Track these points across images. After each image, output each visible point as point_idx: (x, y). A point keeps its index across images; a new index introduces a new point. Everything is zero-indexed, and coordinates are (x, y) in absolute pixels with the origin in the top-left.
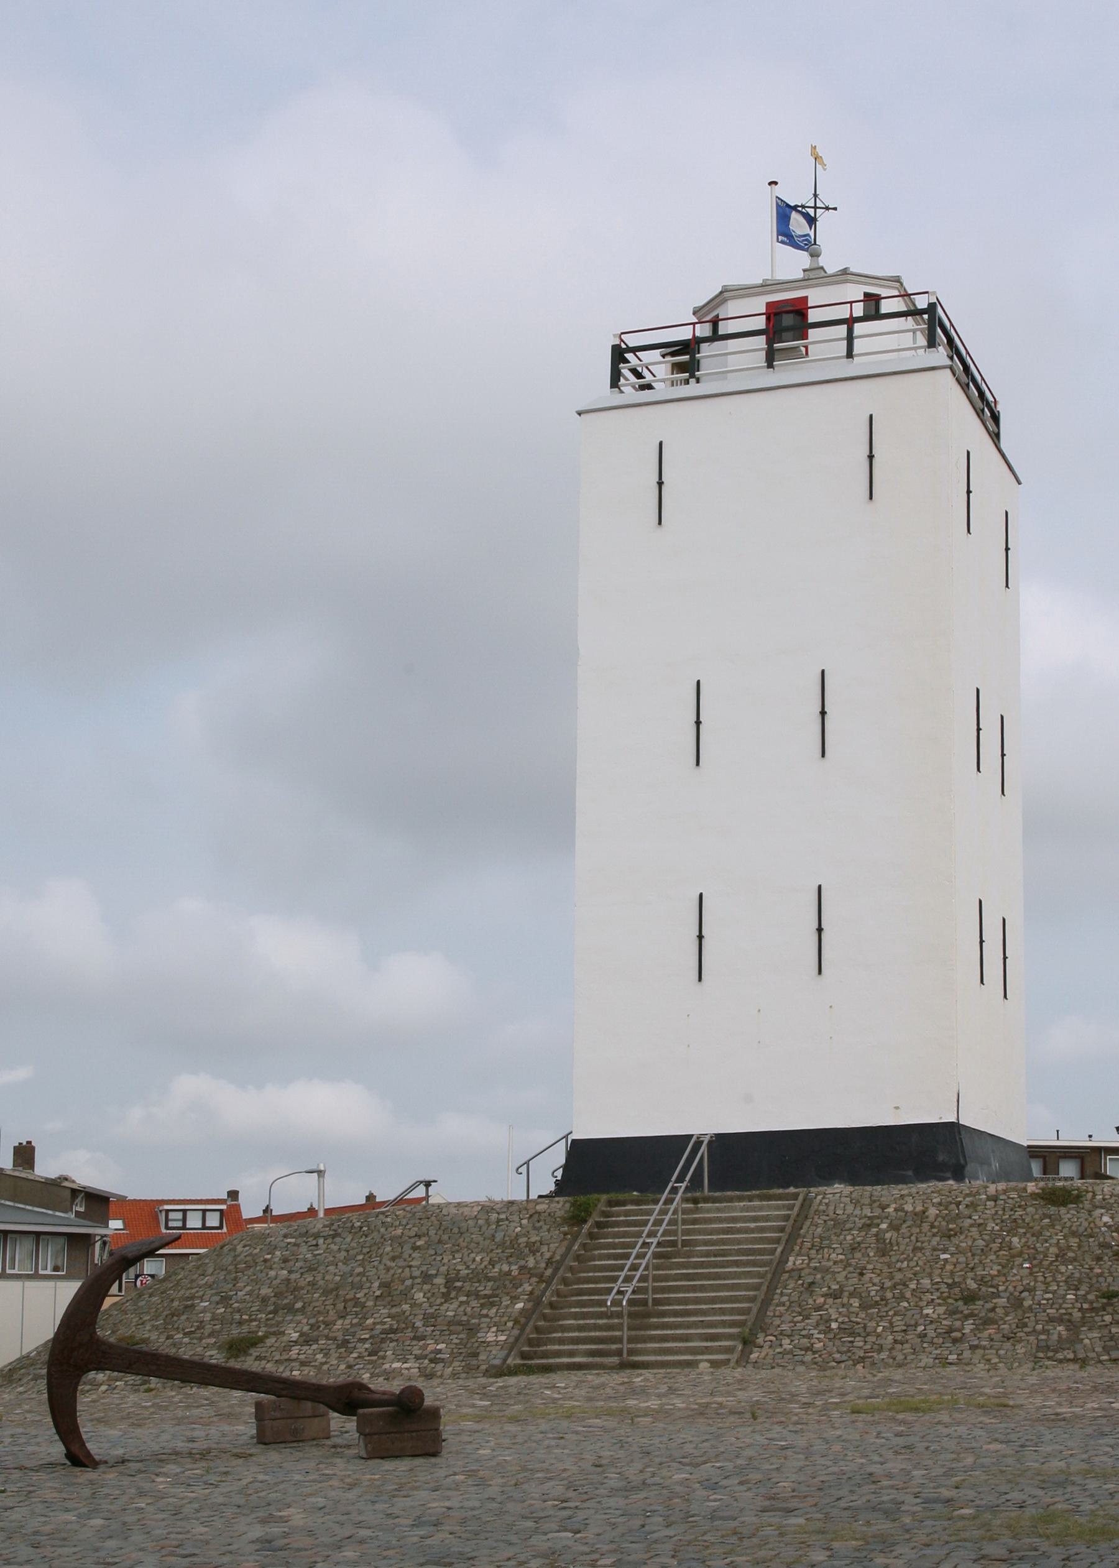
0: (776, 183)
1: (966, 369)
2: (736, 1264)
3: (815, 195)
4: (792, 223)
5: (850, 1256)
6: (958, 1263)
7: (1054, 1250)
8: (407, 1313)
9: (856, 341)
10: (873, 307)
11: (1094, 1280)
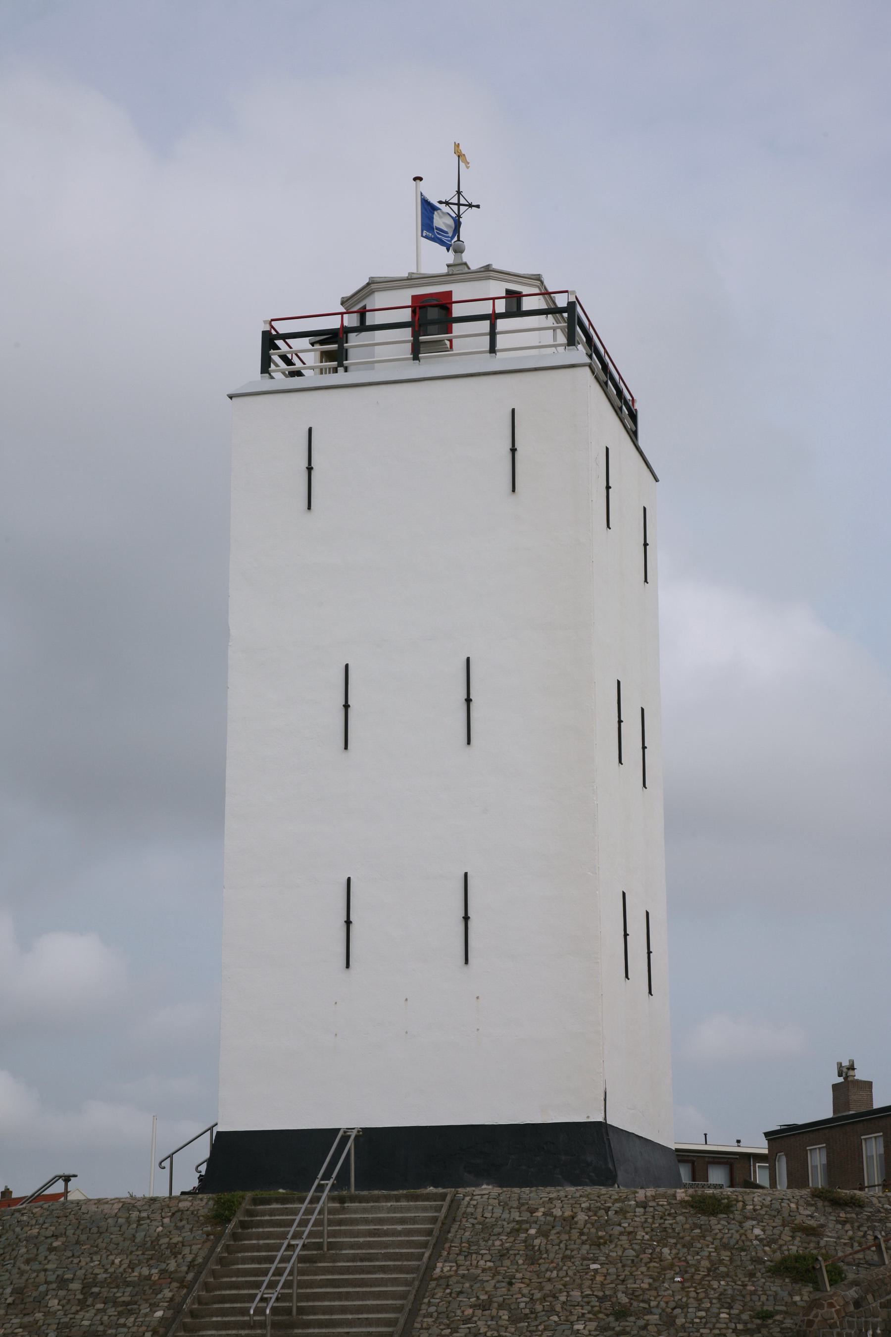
0: (421, 179)
1: (605, 367)
2: (383, 1269)
3: (459, 192)
4: (436, 222)
5: (498, 1263)
6: (608, 1274)
7: (705, 1263)
8: (41, 1323)
9: (498, 337)
10: (514, 304)
11: (748, 1298)
